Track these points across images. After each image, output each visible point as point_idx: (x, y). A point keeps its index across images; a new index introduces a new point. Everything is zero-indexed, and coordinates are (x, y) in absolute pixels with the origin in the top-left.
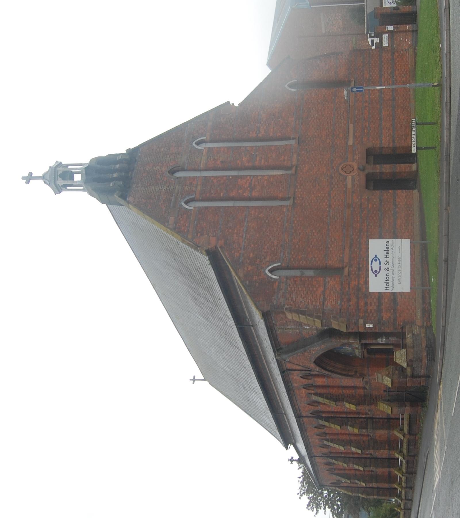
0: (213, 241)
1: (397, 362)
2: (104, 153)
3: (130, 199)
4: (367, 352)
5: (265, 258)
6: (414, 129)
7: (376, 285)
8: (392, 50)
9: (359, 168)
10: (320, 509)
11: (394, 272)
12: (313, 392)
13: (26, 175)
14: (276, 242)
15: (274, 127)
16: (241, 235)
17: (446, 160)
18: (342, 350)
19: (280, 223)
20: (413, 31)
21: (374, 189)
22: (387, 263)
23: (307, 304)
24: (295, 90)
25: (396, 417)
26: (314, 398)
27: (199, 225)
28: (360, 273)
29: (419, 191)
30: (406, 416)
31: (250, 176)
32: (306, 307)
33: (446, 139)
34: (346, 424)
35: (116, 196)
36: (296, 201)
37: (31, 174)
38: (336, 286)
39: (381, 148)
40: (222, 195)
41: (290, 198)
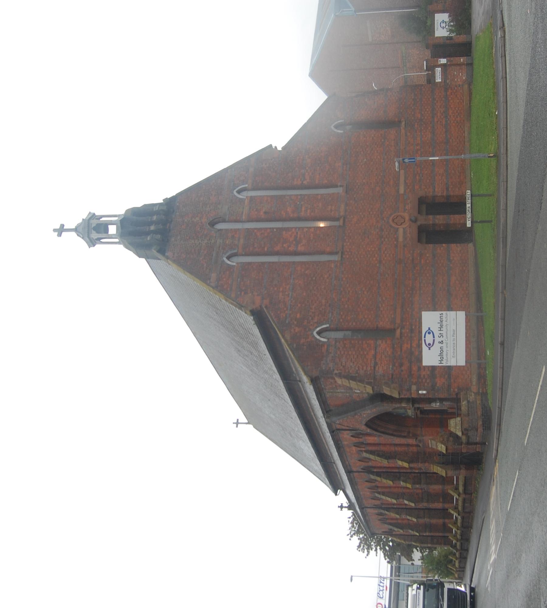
1: (452, 430)
5: (312, 319)
6: (469, 201)
7: (430, 358)
8: (445, 85)
9: (411, 220)
10: (372, 550)
11: (449, 345)
12: (364, 449)
13: (58, 227)
14: (324, 301)
15: (320, 174)
16: (287, 293)
17: (503, 242)
19: (327, 280)
20: (468, 64)
21: (427, 243)
22: (441, 335)
23: (357, 369)
24: (342, 132)
27: (242, 283)
28: (413, 335)
29: (475, 245)
31: (296, 228)
33: (502, 220)
34: (399, 479)
35: (154, 252)
36: (344, 256)
38: (388, 349)
40: (266, 249)
41: (338, 252)
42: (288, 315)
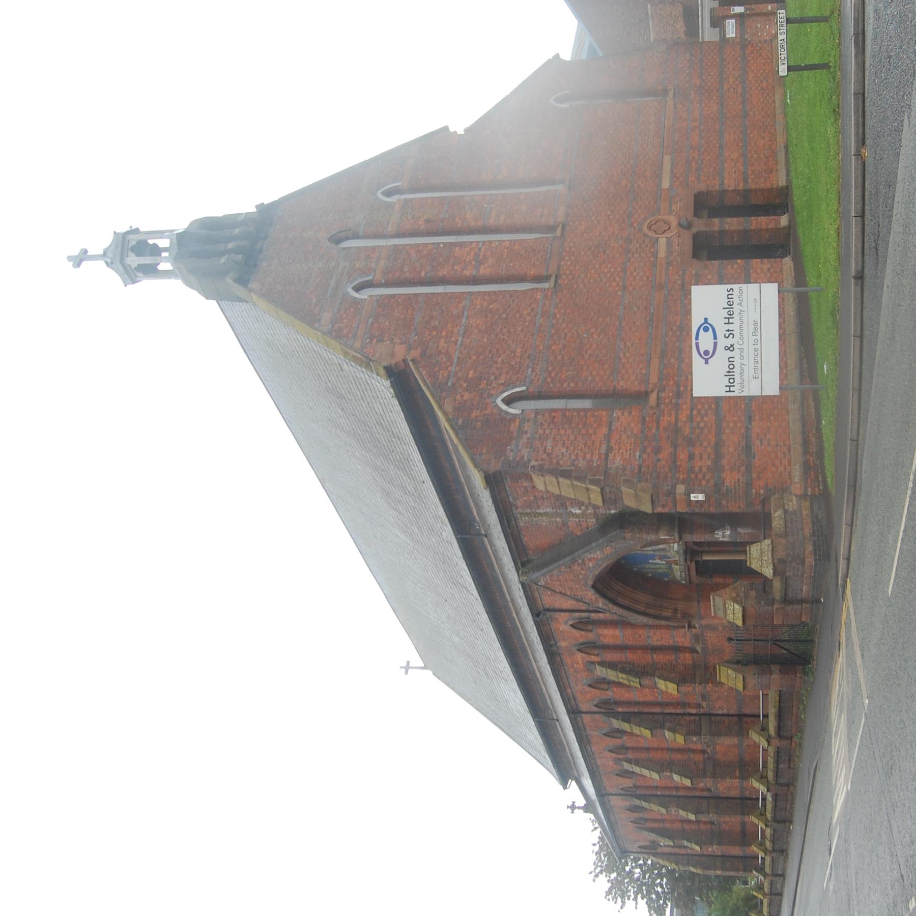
0: (400, 352)
1: (753, 566)
2: (218, 211)
3: (254, 285)
4: (697, 571)
5: (496, 378)
7: (707, 381)
8: (742, 43)
9: (680, 225)
10: (629, 899)
11: (745, 354)
14: (519, 352)
16: (453, 339)
18: (647, 566)
22: (730, 334)
25: (755, 712)
26: (600, 672)
27: (376, 325)
28: (680, 401)
30: (773, 696)
31: (478, 243)
32: (573, 465)
34: (662, 727)
36: (560, 282)
37: (86, 251)
38: (633, 425)
39: (723, 192)
40: (423, 274)
41: (550, 276)
42: (452, 374)
